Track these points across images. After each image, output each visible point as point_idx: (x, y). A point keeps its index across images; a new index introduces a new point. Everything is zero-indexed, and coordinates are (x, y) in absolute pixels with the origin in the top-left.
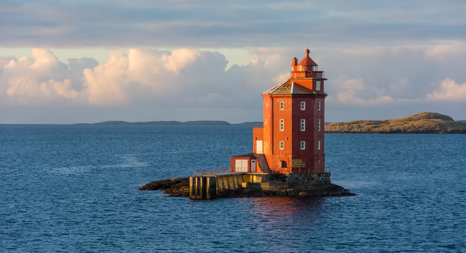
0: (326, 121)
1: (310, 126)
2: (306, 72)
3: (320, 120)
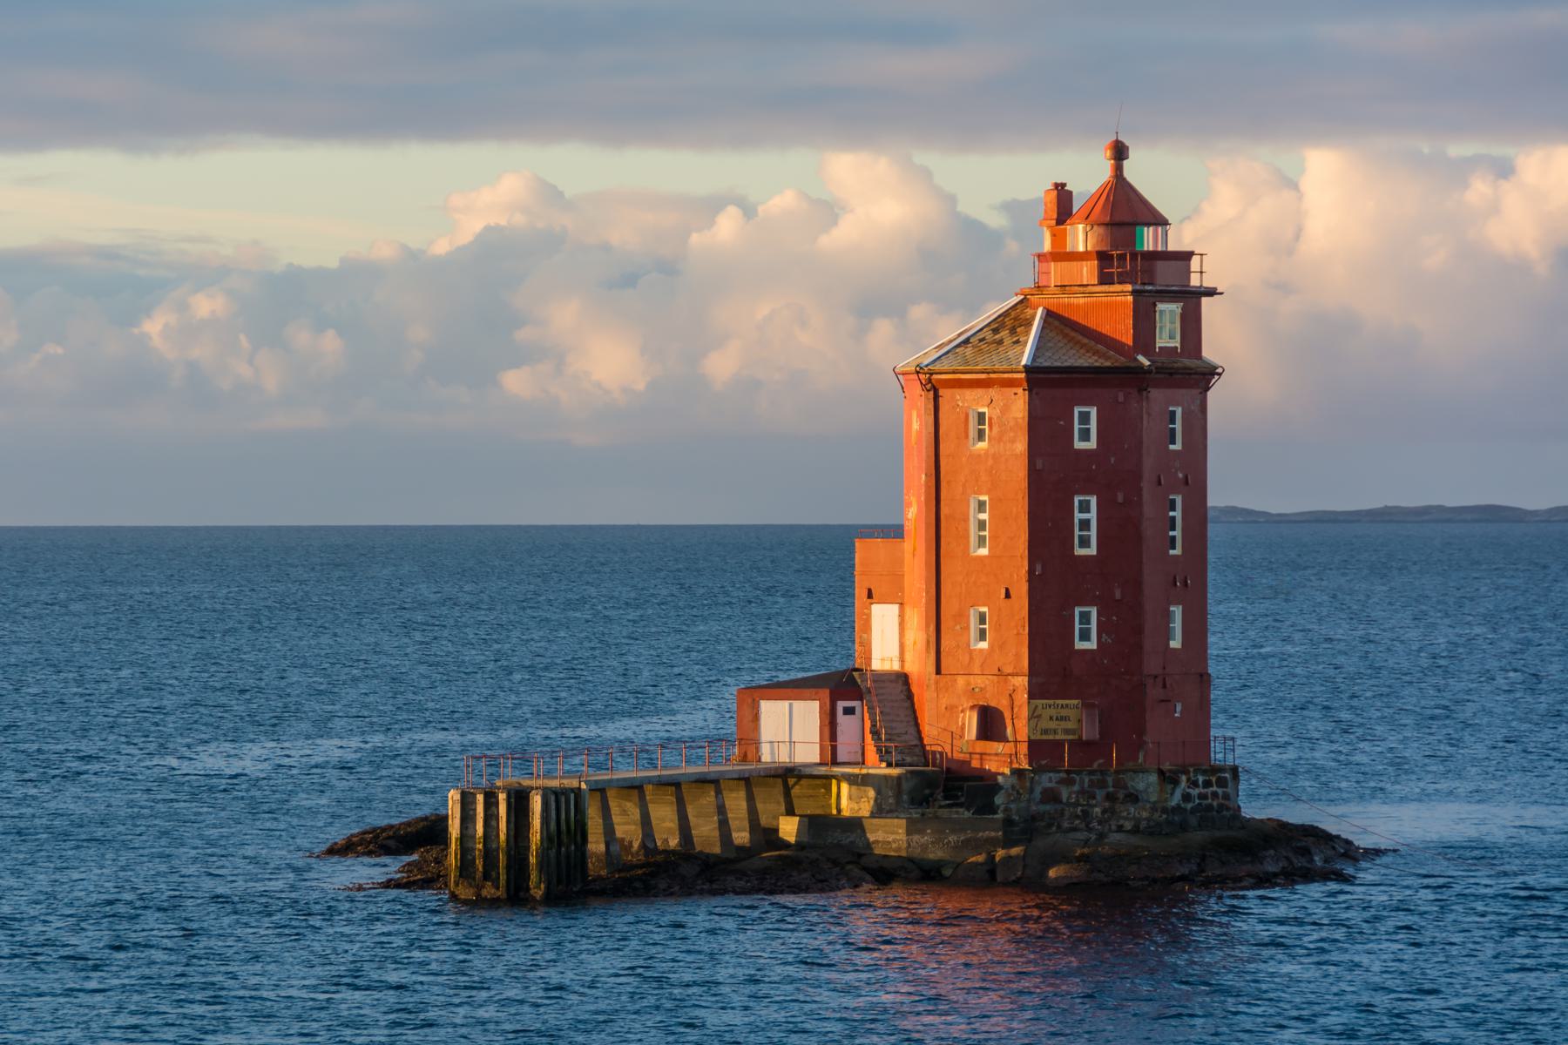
0: (1216, 498)
1: (1122, 530)
2: (1103, 257)
3: (1179, 500)
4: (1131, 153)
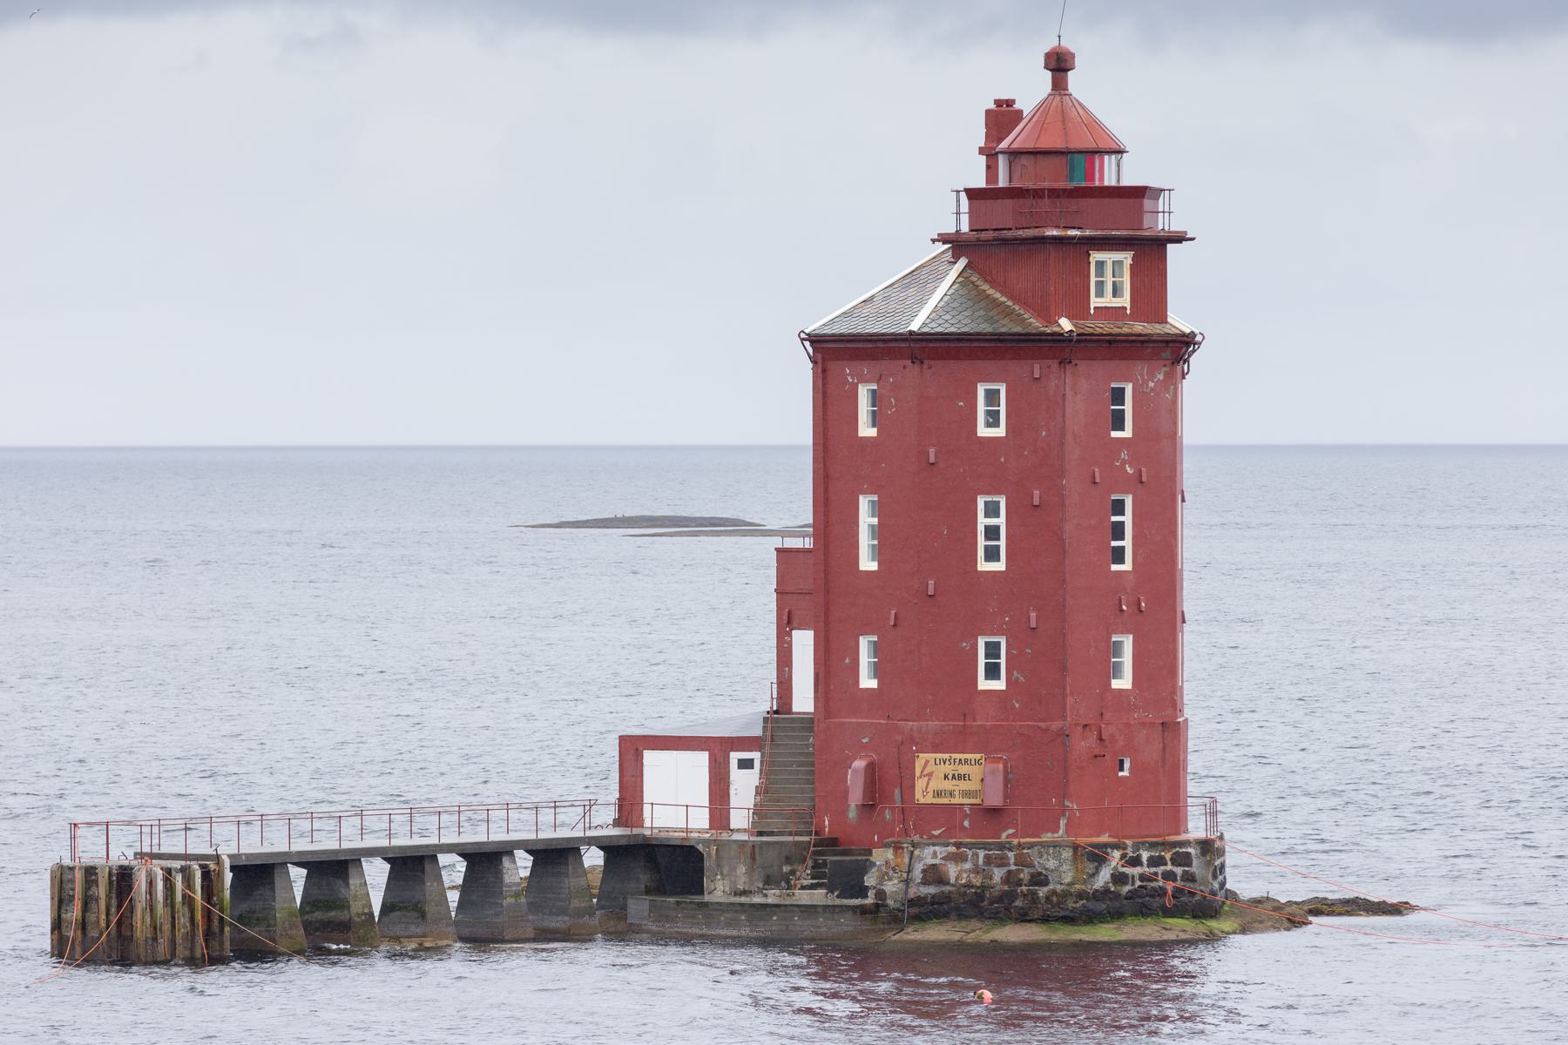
4: (1078, 61)
